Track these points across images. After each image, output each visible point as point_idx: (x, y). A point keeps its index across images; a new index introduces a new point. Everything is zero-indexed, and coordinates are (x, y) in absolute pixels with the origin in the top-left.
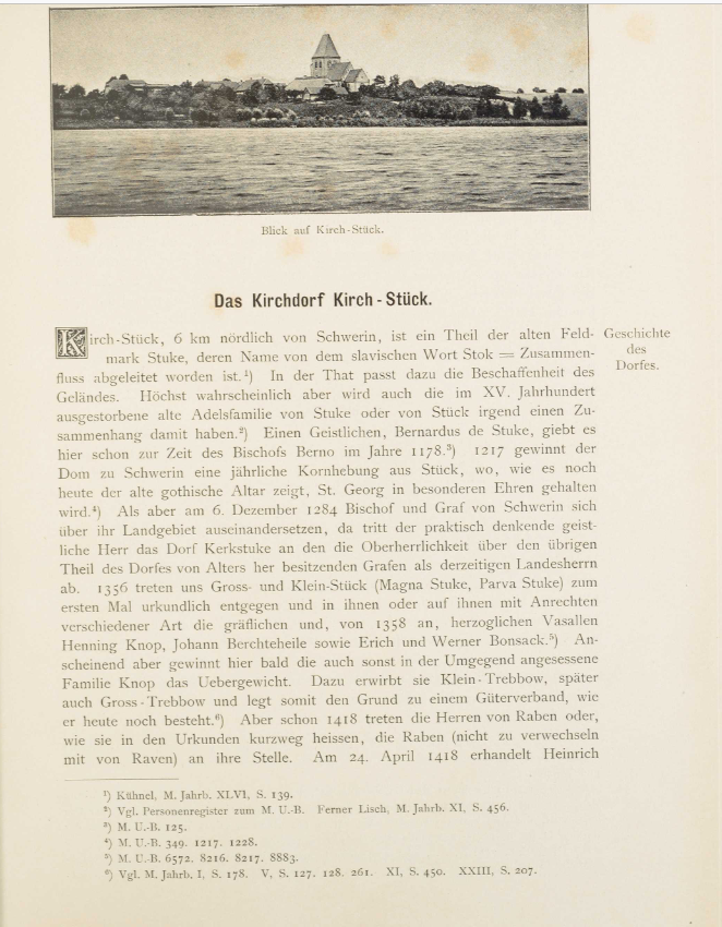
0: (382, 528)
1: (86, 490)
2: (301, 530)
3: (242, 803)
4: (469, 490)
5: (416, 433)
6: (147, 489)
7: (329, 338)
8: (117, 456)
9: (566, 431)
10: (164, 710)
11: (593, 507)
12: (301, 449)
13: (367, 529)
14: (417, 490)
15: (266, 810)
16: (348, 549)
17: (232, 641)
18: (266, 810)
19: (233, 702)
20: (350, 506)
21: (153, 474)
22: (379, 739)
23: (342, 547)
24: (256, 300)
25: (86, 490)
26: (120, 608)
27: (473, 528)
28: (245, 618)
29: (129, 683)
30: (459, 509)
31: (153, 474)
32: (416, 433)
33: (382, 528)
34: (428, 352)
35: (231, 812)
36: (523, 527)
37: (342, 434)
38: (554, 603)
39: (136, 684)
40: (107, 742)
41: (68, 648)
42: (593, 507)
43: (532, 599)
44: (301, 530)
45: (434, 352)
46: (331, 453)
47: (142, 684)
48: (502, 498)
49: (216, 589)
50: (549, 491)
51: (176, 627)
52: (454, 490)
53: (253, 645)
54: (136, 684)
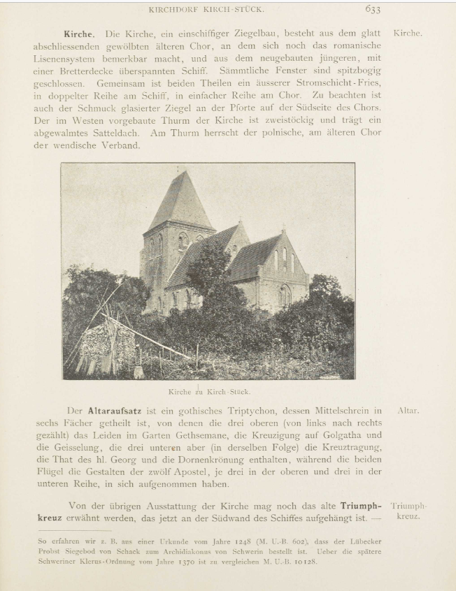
0: (377, 33)
1: (151, 119)
3: (244, 513)
6: (332, 504)
7: (86, 109)
8: (267, 412)
11: (303, 46)
13: (345, 120)
14: (332, 96)
15: (267, 561)
16: (314, 448)
17: (63, 70)
18: (267, 561)
22: (237, 436)
23: (310, 448)
24: (209, 392)
25: (151, 119)
33: (377, 33)
34: (76, 119)
36: (108, 72)
37: (192, 412)
38: (316, 460)
42: (303, 46)
43: (152, 131)
46: (283, 473)
53: (237, 507)
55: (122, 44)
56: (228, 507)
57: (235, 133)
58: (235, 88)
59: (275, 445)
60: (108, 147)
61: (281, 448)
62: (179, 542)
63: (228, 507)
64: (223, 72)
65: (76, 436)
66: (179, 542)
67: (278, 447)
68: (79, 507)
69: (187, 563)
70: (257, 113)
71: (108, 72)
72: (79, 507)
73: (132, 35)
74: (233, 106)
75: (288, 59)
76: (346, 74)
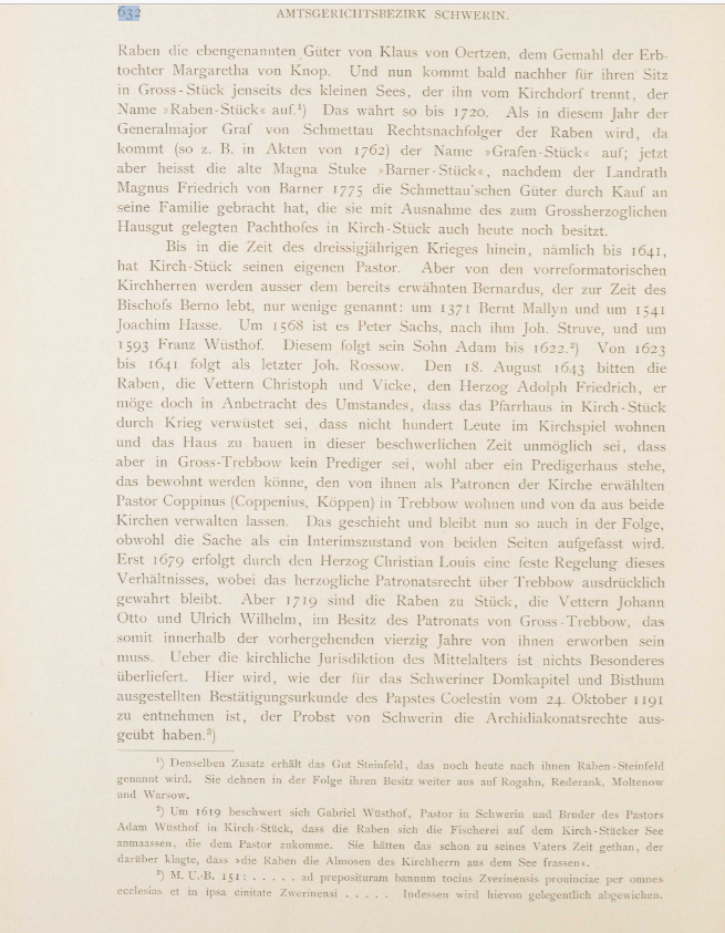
2: (485, 54)
4: (649, 662)
5: (202, 307)
9: (242, 307)
10: (562, 219)
12: (185, 302)
19: (407, 544)
20: (171, 243)
21: (419, 446)
26: (195, 443)
27: (640, 271)
28: (230, 63)
29: (300, 70)
30: (246, 131)
31: (419, 446)
32: (202, 307)
34: (209, 341)
35: (599, 505)
36: (402, 387)
39: (308, 72)
40: (461, 603)
41: (189, 444)
44: (485, 54)
45: (215, 341)
47: (314, 72)
48: (516, 553)
49: (122, 130)
50: (124, 738)
51: (389, 112)
52: (431, 426)
54: (308, 72)
55: (621, 481)
56: (559, 487)
57: (588, 896)
58: (434, 236)
59: (627, 521)
60: (213, 386)
61: (636, 526)
62: (638, 767)
63: (559, 487)
64: (405, 329)
65: (268, 581)
66: (638, 767)
67: (632, 523)
68: (613, 350)
69: (456, 310)
70: (231, 646)
71: (402, 387)
72: (613, 350)
73: (128, 287)
74: (495, 403)
75: (193, 659)
76: (589, 434)
